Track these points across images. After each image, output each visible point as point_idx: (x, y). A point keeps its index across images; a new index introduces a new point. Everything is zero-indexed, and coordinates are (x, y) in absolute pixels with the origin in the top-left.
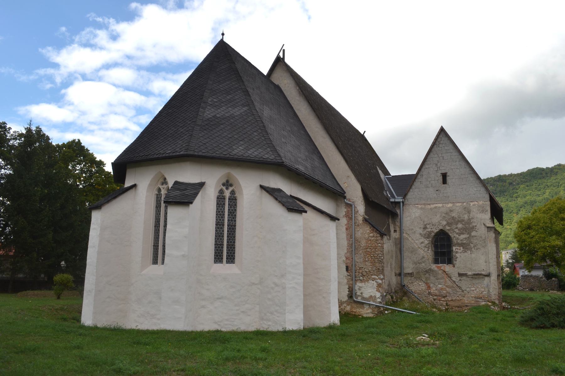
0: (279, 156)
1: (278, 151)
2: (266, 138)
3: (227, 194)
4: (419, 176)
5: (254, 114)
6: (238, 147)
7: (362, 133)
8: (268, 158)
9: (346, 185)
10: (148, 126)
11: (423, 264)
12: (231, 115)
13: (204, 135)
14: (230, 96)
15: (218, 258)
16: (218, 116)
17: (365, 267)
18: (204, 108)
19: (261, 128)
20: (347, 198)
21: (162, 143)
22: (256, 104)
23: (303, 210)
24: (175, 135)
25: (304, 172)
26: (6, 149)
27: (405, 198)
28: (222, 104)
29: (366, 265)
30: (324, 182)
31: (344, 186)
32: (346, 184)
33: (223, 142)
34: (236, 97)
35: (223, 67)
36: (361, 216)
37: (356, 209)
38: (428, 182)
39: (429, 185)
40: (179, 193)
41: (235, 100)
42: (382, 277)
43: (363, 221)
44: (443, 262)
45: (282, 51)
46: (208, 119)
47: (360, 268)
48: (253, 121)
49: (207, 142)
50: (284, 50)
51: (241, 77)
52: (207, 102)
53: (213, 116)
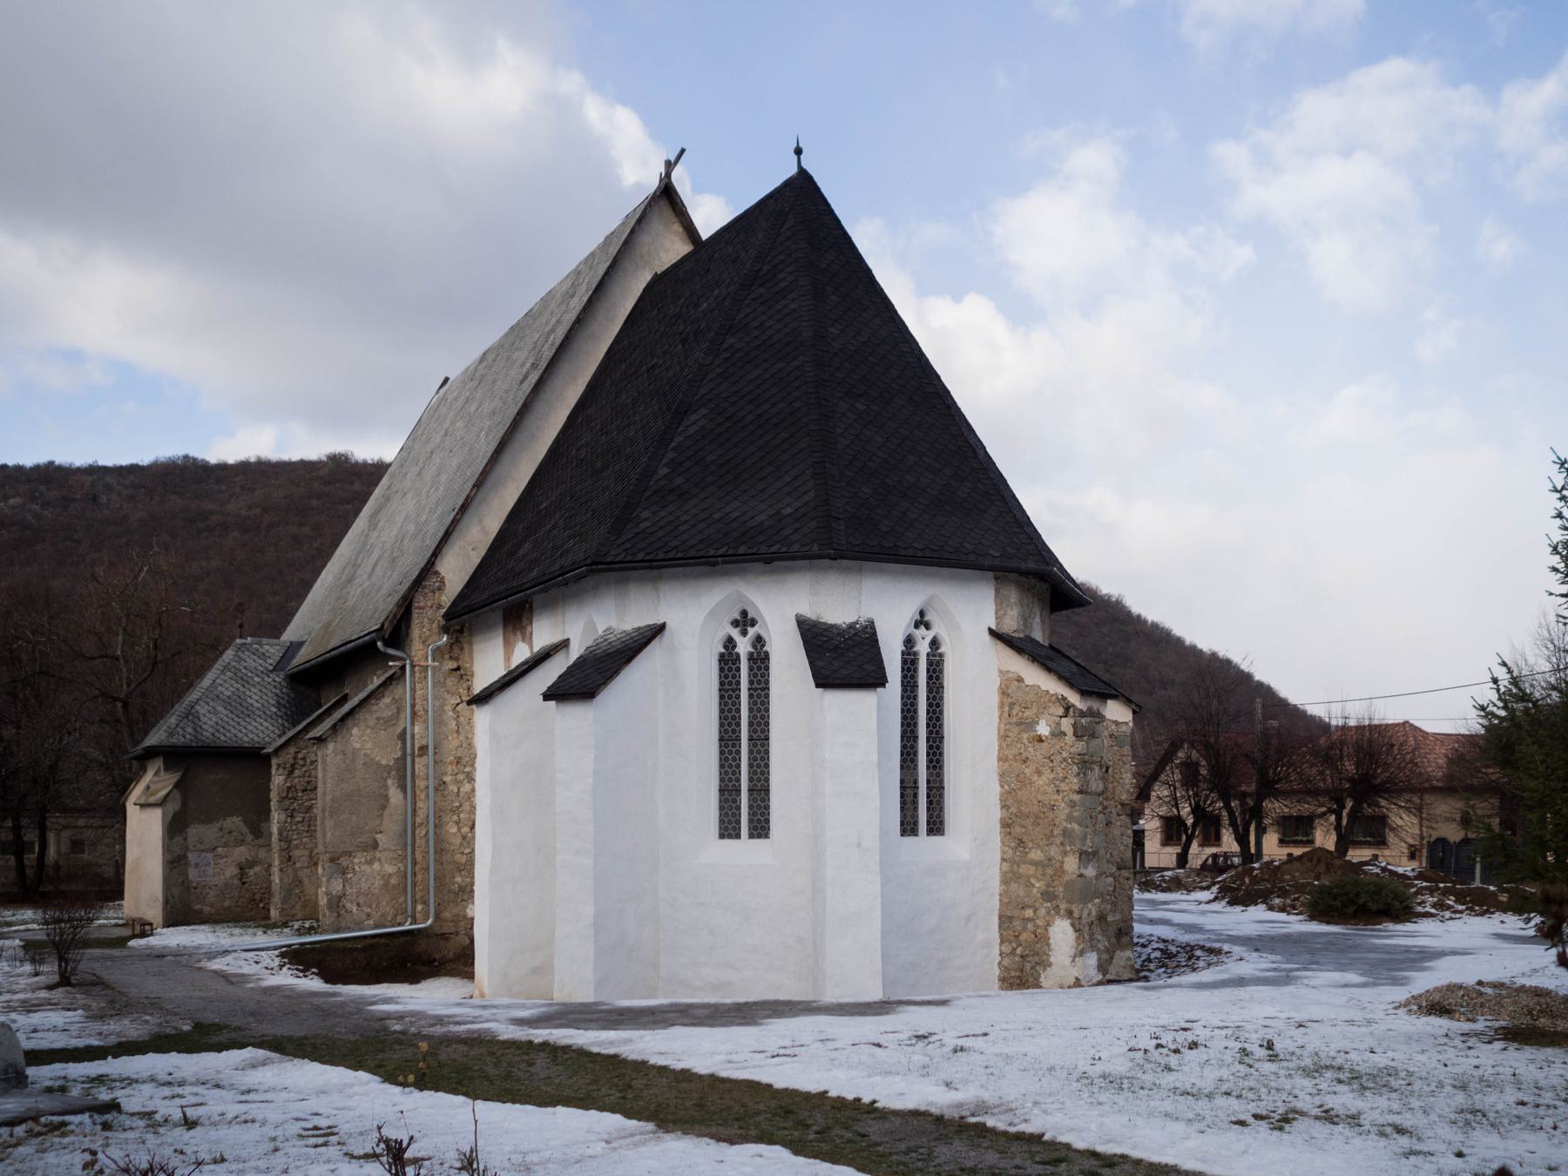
3: (744, 647)
15: (728, 829)
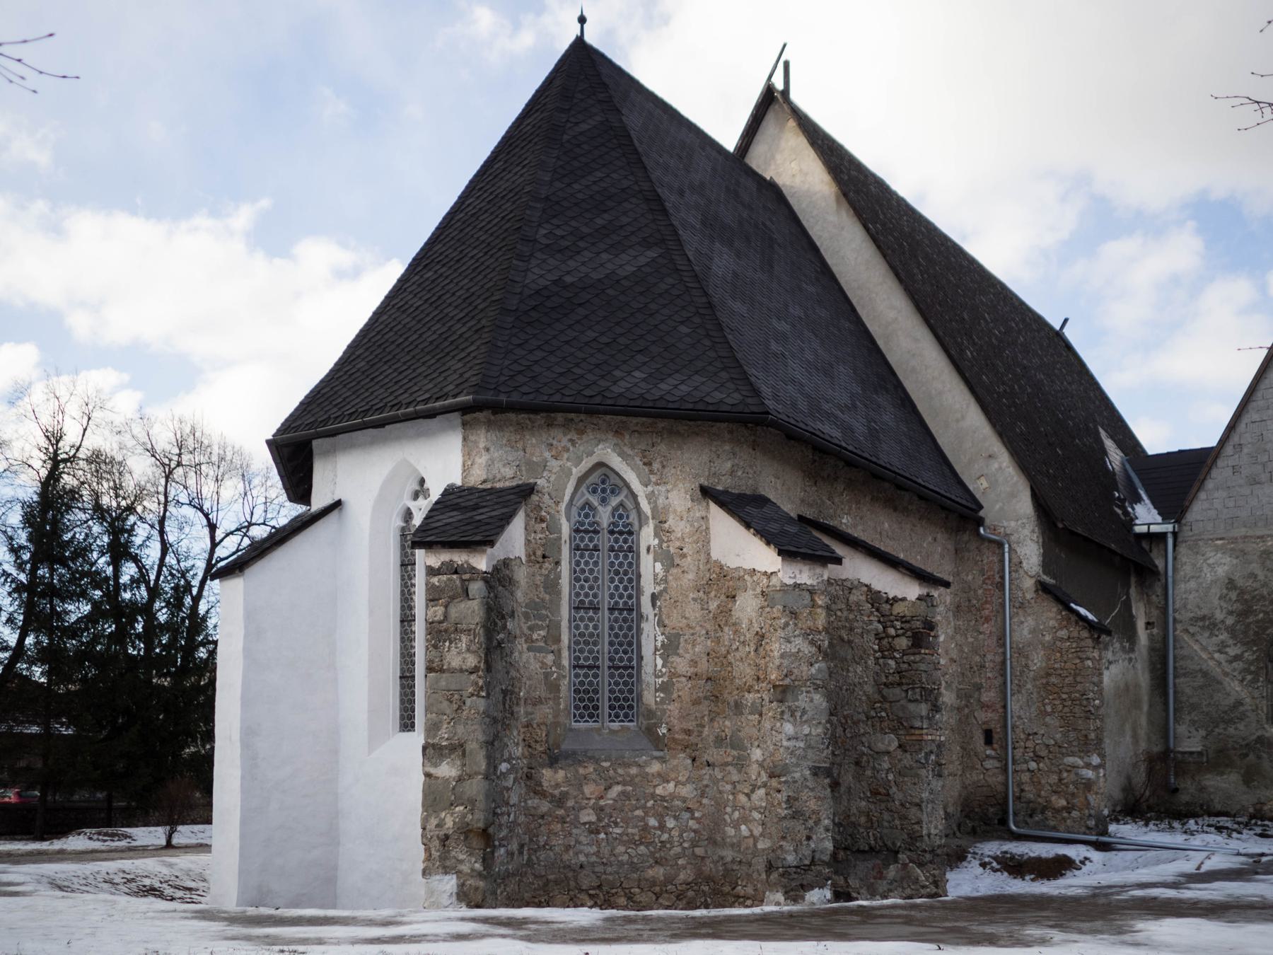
0: (756, 392)
1: (753, 379)
2: (717, 340)
3: (604, 516)
4: (1229, 449)
5: (679, 267)
6: (629, 373)
7: (1057, 327)
8: (721, 401)
9: (985, 484)
10: (366, 325)
11: (1241, 726)
12: (607, 276)
13: (527, 341)
14: (606, 216)
16: (568, 279)
17: (1042, 732)
18: (526, 259)
19: (701, 311)
20: (987, 522)
21: (405, 374)
22: (684, 235)
23: (829, 554)
24: (442, 347)
25: (837, 442)
27: (1183, 521)
28: (582, 244)
29: (1047, 725)
30: (908, 475)
31: (978, 487)
32: (983, 480)
33: (584, 359)
34: (625, 220)
35: (584, 127)
36: (1031, 577)
37: (1014, 556)
38: (1260, 467)
39: (1263, 476)
40: (460, 517)
41: (621, 227)
42: (1095, 760)
43: (1036, 591)
45: (781, 65)
46: (537, 292)
47: (1029, 735)
48: (675, 292)
49: (536, 362)
50: (787, 65)
51: (636, 151)
52: (535, 240)
53: (555, 282)
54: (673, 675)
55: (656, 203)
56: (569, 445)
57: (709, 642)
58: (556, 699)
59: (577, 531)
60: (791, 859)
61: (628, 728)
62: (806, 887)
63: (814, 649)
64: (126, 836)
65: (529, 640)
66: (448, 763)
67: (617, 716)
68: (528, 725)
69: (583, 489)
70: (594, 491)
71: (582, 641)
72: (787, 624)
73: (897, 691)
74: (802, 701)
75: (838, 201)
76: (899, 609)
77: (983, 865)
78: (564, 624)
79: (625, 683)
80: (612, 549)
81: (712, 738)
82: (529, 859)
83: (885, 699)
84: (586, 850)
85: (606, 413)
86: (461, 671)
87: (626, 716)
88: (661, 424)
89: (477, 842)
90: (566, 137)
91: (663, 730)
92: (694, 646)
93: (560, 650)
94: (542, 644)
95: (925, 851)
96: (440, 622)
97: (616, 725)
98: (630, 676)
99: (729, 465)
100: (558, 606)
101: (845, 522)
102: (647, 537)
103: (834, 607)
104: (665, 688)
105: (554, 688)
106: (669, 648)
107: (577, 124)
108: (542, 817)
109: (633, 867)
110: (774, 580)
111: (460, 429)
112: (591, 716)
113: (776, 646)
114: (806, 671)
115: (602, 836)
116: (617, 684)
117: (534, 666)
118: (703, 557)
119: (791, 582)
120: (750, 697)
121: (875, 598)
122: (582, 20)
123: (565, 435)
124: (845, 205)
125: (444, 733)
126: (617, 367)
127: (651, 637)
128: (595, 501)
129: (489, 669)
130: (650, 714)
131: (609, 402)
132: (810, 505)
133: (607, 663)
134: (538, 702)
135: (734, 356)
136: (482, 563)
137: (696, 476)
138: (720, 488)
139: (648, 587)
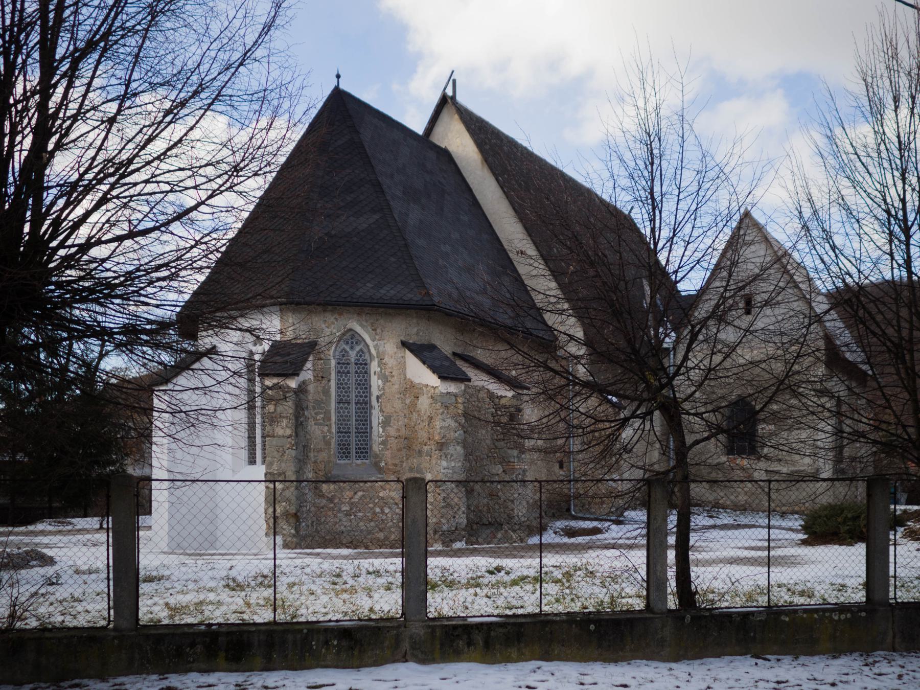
3: (353, 355)
6: (365, 284)
16: (333, 232)
26: (787, 619)
44: (741, 452)
50: (454, 81)
54: (387, 436)
55: (378, 187)
56: (334, 321)
57: (406, 420)
58: (329, 449)
59: (339, 363)
60: (445, 528)
61: (365, 463)
62: (452, 541)
63: (457, 424)
64: (71, 524)
65: (315, 419)
66: (267, 487)
67: (360, 457)
68: (315, 462)
69: (342, 342)
70: (347, 343)
71: (342, 420)
72: (443, 413)
73: (502, 443)
74: (451, 450)
75: (482, 164)
76: (503, 401)
77: (555, 533)
78: (333, 411)
79: (364, 440)
80: (356, 372)
81: (407, 468)
82: (316, 529)
83: (496, 447)
84: (345, 524)
85: (353, 306)
86: (283, 436)
87: (364, 457)
88: (381, 310)
89: (292, 520)
90: (330, 149)
91: (383, 464)
92: (398, 421)
93: (331, 425)
94: (322, 421)
95: (515, 524)
96: (273, 413)
97: (359, 462)
98: (366, 437)
99: (415, 330)
100: (330, 402)
101: (481, 355)
102: (374, 367)
103: (471, 400)
104: (384, 443)
105: (328, 443)
106: (386, 423)
107: (336, 141)
108: (322, 508)
109: (369, 533)
110: (437, 391)
111: (278, 314)
112: (347, 457)
113: (438, 423)
114: (453, 435)
115: (353, 517)
116: (359, 441)
117: (318, 432)
118: (402, 376)
119: (445, 391)
120: (426, 448)
121: (491, 395)
122: (338, 76)
123: (332, 315)
124: (486, 166)
125: (275, 467)
126: (358, 281)
127: (376, 417)
128: (347, 348)
129: (297, 435)
130: (376, 456)
131: (355, 301)
132: (459, 346)
133: (355, 430)
134: (320, 450)
135: (418, 274)
136: (293, 384)
137: (399, 336)
138: (411, 341)
139: (375, 392)
